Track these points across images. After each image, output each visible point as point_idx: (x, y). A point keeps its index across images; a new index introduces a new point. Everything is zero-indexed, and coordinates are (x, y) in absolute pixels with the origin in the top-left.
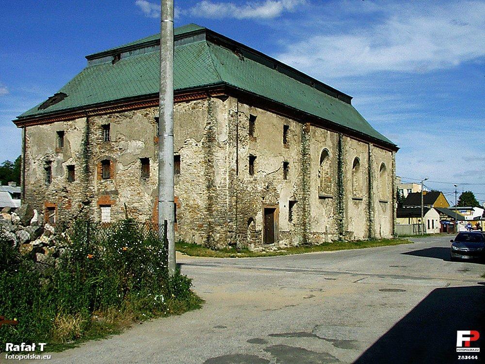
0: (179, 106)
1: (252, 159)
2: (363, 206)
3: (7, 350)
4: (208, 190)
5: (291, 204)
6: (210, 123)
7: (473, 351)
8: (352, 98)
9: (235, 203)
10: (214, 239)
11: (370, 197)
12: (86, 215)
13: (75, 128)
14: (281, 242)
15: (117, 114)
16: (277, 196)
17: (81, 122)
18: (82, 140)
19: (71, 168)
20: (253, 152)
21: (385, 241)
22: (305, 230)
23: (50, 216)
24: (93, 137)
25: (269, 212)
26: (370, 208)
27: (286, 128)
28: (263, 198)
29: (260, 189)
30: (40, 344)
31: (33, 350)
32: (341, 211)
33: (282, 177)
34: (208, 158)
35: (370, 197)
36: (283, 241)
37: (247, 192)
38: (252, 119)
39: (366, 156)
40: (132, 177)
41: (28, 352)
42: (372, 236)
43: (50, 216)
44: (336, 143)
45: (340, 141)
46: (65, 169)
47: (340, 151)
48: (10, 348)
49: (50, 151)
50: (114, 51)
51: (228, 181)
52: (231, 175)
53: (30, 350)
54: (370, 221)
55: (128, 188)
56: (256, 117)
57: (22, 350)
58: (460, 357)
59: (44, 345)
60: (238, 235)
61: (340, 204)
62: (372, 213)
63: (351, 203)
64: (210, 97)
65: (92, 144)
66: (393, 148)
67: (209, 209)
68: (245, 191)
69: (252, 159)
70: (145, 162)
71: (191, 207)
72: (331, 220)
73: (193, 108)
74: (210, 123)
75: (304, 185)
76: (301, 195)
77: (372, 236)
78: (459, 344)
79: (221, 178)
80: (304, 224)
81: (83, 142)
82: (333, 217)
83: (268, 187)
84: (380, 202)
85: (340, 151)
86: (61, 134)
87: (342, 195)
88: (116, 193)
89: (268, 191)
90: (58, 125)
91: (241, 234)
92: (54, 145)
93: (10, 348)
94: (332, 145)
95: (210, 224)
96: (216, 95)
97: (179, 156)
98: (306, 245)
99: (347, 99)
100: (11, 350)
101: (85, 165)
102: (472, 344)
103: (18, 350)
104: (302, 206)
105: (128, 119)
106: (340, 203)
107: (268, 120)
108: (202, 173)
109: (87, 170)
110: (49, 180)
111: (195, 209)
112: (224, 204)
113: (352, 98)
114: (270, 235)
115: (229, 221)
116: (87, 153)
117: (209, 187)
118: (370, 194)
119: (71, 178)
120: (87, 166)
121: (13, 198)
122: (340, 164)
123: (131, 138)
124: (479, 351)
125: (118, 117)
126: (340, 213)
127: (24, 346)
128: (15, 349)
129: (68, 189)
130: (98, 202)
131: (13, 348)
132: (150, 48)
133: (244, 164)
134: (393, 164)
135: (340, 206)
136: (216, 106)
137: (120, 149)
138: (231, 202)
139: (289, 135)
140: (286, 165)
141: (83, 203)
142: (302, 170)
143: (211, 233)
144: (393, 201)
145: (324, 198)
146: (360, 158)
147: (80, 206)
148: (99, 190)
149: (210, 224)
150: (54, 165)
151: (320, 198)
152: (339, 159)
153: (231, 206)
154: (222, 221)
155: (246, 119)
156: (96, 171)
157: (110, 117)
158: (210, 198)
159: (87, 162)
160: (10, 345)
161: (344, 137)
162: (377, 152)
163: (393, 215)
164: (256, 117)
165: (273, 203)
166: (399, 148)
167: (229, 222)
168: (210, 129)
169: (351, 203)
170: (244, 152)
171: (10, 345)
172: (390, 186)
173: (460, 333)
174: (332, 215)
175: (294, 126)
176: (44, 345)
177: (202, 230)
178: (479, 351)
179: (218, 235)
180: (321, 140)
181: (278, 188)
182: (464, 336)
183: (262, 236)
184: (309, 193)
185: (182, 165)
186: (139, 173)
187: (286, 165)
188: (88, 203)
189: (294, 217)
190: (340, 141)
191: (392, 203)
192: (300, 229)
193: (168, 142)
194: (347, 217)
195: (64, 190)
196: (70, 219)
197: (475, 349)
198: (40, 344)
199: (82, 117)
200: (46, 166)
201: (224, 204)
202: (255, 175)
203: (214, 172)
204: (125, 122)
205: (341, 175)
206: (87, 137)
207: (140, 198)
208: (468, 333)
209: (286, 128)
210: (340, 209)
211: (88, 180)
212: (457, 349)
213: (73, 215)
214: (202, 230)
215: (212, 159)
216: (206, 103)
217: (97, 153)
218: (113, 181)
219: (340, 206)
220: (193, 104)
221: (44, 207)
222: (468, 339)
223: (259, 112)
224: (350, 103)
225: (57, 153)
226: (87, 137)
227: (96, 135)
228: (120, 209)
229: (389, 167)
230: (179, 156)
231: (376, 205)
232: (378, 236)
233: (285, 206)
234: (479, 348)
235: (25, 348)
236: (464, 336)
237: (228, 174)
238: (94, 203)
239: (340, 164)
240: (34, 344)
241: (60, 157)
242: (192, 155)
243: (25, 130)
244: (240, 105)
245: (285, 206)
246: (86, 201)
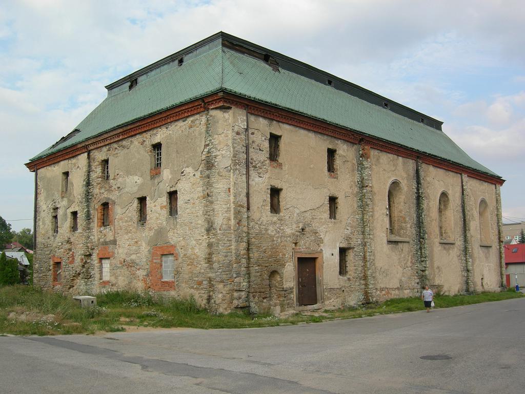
0: (175, 126)
1: (275, 192)
2: (455, 252)
4: (208, 234)
5: (343, 252)
6: (208, 145)
8: (442, 123)
9: (245, 251)
10: (215, 301)
11: (466, 240)
12: (87, 271)
13: (78, 167)
14: (327, 302)
15: (115, 145)
16: (319, 241)
17: (83, 159)
18: (84, 181)
19: (75, 214)
20: (278, 185)
21: (488, 296)
22: (366, 285)
23: (58, 273)
24: (93, 175)
25: (307, 264)
26: (466, 254)
27: (331, 153)
28: (296, 244)
29: (288, 231)
32: (423, 259)
33: (326, 215)
34: (207, 191)
35: (466, 240)
36: (331, 301)
37: (266, 236)
38: (274, 139)
39: (459, 189)
40: (129, 221)
42: (471, 289)
43: (58, 273)
44: (412, 172)
45: (417, 172)
46: (69, 215)
47: (418, 183)
49: (57, 196)
50: (130, 76)
51: (233, 222)
52: (237, 213)
54: (468, 271)
55: (127, 237)
56: (280, 137)
60: (251, 295)
61: (421, 250)
62: (470, 260)
63: (437, 249)
64: (208, 109)
65: (92, 185)
66: (497, 181)
67: (209, 260)
68: (264, 234)
69: (275, 192)
70: (142, 200)
71: (189, 258)
72: (409, 271)
73: (191, 127)
74: (208, 145)
75: (364, 226)
76: (359, 240)
77: (471, 289)
79: (223, 216)
80: (365, 277)
81: (85, 183)
82: (411, 267)
83: (303, 229)
85: (418, 183)
86: (66, 174)
87: (423, 239)
88: (114, 242)
89: (304, 234)
90: (63, 166)
91: (258, 294)
92: (60, 189)
94: (405, 176)
95: (210, 280)
96: (214, 107)
97: (175, 192)
98: (368, 303)
99: (437, 125)
101: (86, 210)
104: (361, 254)
105: (126, 151)
106: (421, 248)
107: (301, 146)
108: (201, 212)
109: (88, 217)
110: (56, 230)
111: (192, 262)
112: (228, 252)
113: (442, 123)
114: (308, 290)
115: (235, 276)
116: (88, 196)
117: (208, 231)
118: (465, 236)
119: (74, 228)
120: (88, 211)
122: (419, 198)
123: (129, 173)
125: (116, 148)
126: (422, 261)
129: (72, 240)
130: (98, 254)
132: (166, 67)
133: (261, 199)
134: (497, 200)
135: (421, 253)
136: (215, 121)
137: (119, 188)
138: (237, 250)
139: (338, 162)
140: (333, 200)
141: (85, 256)
142: (360, 207)
143: (211, 293)
144: (500, 245)
145: (396, 242)
146: (450, 192)
147: (82, 259)
148: (99, 240)
149: (211, 281)
150: (60, 213)
151: (390, 242)
152: (418, 193)
153: (238, 256)
154: (225, 276)
155: (263, 138)
156: (96, 215)
157: (109, 150)
158: (210, 245)
159: (88, 206)
161: (424, 166)
162: (472, 185)
163: (501, 263)
164: (280, 137)
165: (313, 250)
166: (504, 181)
167: (235, 278)
168: (209, 152)
169: (437, 249)
170: (261, 183)
172: (495, 226)
174: (409, 264)
175: (345, 151)
177: (202, 289)
179: (220, 295)
180: (386, 170)
181: (322, 230)
183: (294, 296)
184: (371, 236)
185: (180, 202)
186: (135, 216)
187: (333, 200)
188: (90, 255)
189: (350, 267)
190: (417, 172)
191: (498, 247)
192: (358, 285)
193: (166, 174)
194: (432, 266)
195: (69, 242)
196: (74, 276)
199: (84, 153)
200: (54, 214)
201: (228, 252)
202: (281, 214)
203: (213, 210)
204: (122, 153)
205: (422, 213)
206: (89, 176)
207: (137, 248)
209: (331, 153)
210: (421, 255)
211: (89, 229)
213: (76, 271)
214: (202, 289)
215: (211, 192)
216: (204, 119)
217: (97, 195)
218: (112, 228)
219: (421, 253)
220: (190, 122)
221: (52, 263)
223: (285, 131)
224: (440, 129)
225: (63, 197)
226: (89, 176)
227: (96, 172)
228: (119, 262)
229: (492, 205)
230: (175, 192)
231: (477, 251)
232: (479, 289)
233: (332, 255)
237: (232, 212)
238: (95, 257)
239: (419, 198)
241: (65, 202)
242: (190, 190)
243: (36, 175)
244: (252, 118)
245: (332, 255)
246: (88, 253)
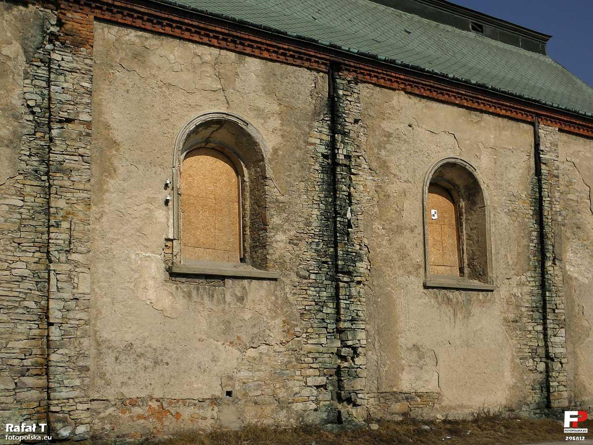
3: (7, 430)
7: (581, 432)
30: (40, 425)
31: (34, 431)
41: (29, 433)
48: (11, 428)
53: (31, 431)
57: (23, 431)
58: (567, 437)
59: (45, 426)
78: (567, 424)
84: (426, 287)
93: (11, 428)
100: (11, 431)
102: (579, 425)
103: (19, 431)
121: (429, 192)
124: (587, 432)
127: (25, 426)
128: (15, 430)
160: (10, 426)
171: (10, 426)
173: (567, 414)
176: (45, 426)
178: (587, 432)
182: (571, 416)
197: (582, 429)
208: (576, 413)
212: (565, 429)
222: (576, 420)
234: (587, 429)
235: (25, 428)
236: (571, 416)
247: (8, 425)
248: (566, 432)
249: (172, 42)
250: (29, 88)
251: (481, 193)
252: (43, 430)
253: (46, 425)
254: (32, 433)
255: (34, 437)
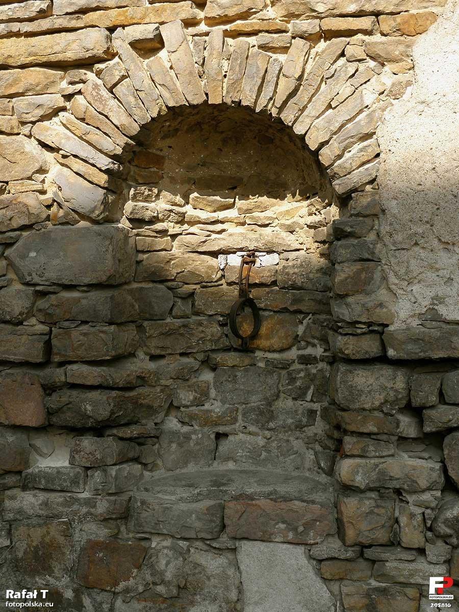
30: (41, 591)
31: (35, 597)
48: (11, 595)
57: (23, 597)
58: (432, 604)
78: (432, 591)
93: (11, 595)
103: (19, 597)
128: (15, 597)
131: (13, 595)
160: (10, 593)
171: (10, 593)
173: (433, 580)
182: (437, 583)
198: (41, 591)
208: (441, 579)
222: (441, 586)
235: (26, 595)
236: (437, 583)
240: (35, 591)
247: (8, 591)
248: (431, 599)
249: (381, 369)
250: (20, 15)
251: (338, 204)
252: (44, 597)
253: (47, 591)
254: (33, 600)
255: (35, 604)
